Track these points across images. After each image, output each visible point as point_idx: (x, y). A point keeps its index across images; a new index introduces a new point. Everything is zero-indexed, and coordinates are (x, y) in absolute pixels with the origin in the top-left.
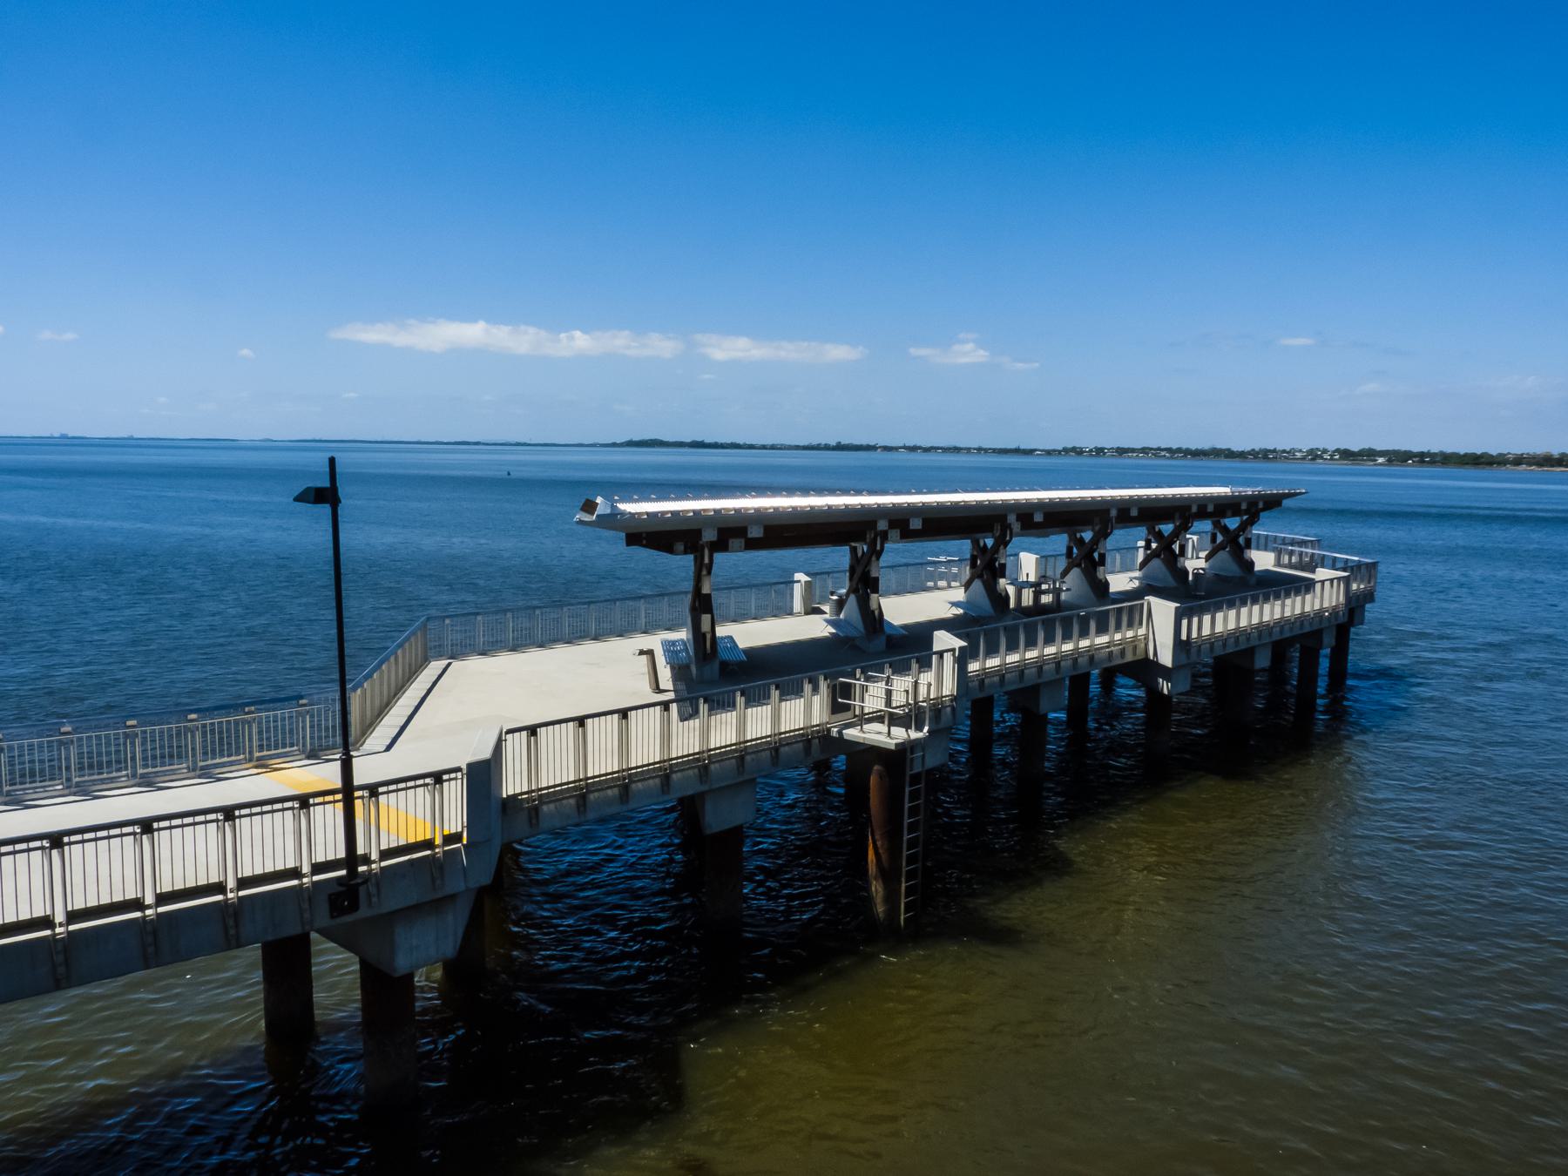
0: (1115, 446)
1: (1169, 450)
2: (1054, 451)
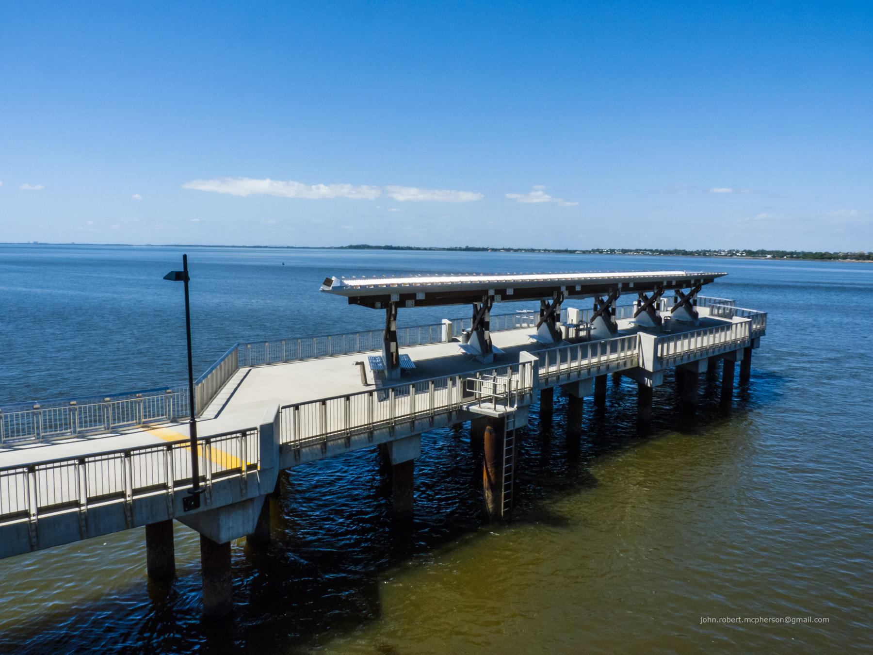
0: (621, 249)
1: (651, 251)
2: (587, 251)
